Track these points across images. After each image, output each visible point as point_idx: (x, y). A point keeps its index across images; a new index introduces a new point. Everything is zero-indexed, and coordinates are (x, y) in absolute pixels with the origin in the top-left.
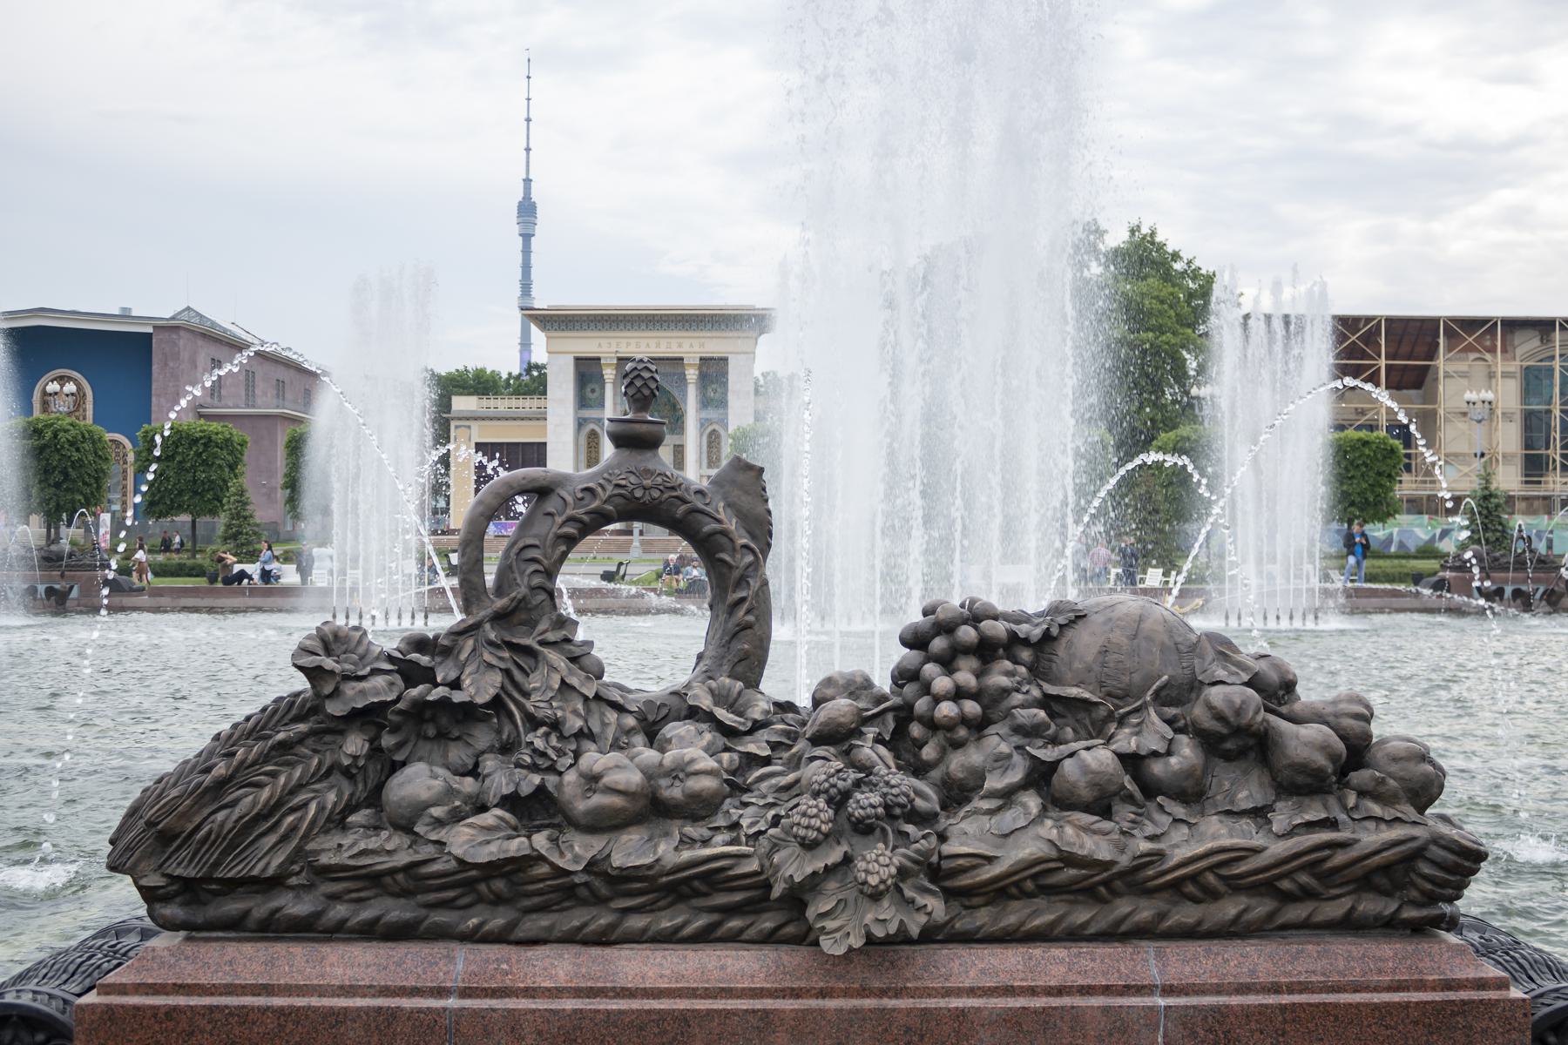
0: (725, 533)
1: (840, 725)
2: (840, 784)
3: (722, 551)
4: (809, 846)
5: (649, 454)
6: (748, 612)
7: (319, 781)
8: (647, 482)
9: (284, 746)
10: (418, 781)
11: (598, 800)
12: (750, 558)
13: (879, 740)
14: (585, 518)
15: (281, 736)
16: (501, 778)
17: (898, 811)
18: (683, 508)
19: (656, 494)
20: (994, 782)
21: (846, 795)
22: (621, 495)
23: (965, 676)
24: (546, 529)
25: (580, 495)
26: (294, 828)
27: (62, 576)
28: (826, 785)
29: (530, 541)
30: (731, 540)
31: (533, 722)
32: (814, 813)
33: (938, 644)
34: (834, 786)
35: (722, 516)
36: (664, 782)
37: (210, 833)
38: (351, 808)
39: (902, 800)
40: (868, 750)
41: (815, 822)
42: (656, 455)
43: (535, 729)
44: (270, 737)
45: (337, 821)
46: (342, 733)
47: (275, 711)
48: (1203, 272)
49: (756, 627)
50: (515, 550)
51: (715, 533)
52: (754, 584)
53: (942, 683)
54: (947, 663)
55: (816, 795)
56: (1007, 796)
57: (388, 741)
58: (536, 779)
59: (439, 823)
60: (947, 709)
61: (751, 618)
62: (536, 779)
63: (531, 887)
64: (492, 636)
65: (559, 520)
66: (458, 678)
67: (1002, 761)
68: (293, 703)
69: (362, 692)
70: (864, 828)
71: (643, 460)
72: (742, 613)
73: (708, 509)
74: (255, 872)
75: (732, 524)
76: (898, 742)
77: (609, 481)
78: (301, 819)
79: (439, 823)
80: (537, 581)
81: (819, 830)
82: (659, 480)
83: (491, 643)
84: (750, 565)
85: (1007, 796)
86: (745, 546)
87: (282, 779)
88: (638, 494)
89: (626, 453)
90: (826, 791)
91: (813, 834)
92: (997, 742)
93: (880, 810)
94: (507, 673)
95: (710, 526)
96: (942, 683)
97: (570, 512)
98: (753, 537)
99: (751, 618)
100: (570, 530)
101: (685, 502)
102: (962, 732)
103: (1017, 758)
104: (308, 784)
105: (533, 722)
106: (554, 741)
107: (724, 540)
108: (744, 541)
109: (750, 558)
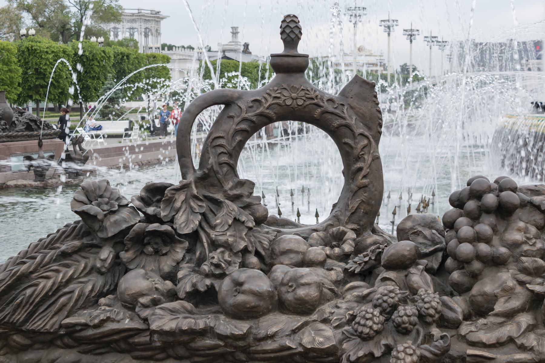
0: (347, 126)
1: (404, 256)
2: (390, 300)
3: (345, 137)
4: (365, 338)
5: (298, 75)
6: (365, 177)
7: (85, 276)
8: (294, 95)
9: (65, 255)
10: (136, 281)
11: (241, 298)
12: (366, 142)
13: (428, 270)
14: (254, 119)
15: (63, 247)
16: (188, 279)
17: (429, 319)
18: (319, 110)
19: (300, 102)
20: (499, 307)
21: (394, 307)
22: (277, 104)
23: (484, 228)
24: (231, 126)
25: (251, 104)
26: (64, 305)
27: (40, 145)
28: (380, 301)
29: (217, 135)
30: (352, 130)
31: (214, 245)
32: (371, 316)
33: (471, 205)
34: (385, 302)
35: (346, 115)
36: (283, 289)
37: (22, 301)
38: (102, 294)
39: (432, 311)
40: (417, 276)
41: (369, 323)
42: (303, 77)
43: (216, 249)
44: (59, 248)
45: (92, 301)
46: (101, 247)
47: (64, 232)
48: (231, 31)
49: (370, 186)
50: (210, 140)
51: (341, 126)
52: (368, 158)
53: (466, 230)
54: (475, 218)
55: (375, 306)
56: (510, 315)
57: (125, 256)
58: (208, 282)
59: (145, 306)
60: (466, 248)
61: (365, 181)
62: (208, 282)
63: (257, 356)
64: (195, 191)
65: (237, 120)
66: (200, 214)
67: (508, 292)
68: (76, 227)
69: (116, 223)
70: (403, 331)
71: (294, 80)
72: (360, 178)
73: (337, 111)
74: (48, 327)
75: (352, 121)
76: (438, 272)
77: (270, 95)
78: (70, 299)
79: (145, 306)
80: (224, 158)
81: (371, 328)
82: (303, 93)
83: (196, 197)
84: (365, 147)
85: (510, 315)
86: (362, 134)
87: (61, 275)
88: (289, 102)
89: (280, 75)
90: (380, 305)
91: (367, 330)
92: (507, 277)
93: (414, 319)
94: (203, 215)
95: (337, 122)
96: (466, 230)
97: (244, 115)
98: (369, 128)
99: (365, 181)
100: (243, 126)
101: (319, 106)
102: (477, 265)
103: (519, 289)
104: (78, 278)
105: (214, 245)
106: (227, 257)
107: (347, 131)
108: (361, 131)
109: (366, 142)
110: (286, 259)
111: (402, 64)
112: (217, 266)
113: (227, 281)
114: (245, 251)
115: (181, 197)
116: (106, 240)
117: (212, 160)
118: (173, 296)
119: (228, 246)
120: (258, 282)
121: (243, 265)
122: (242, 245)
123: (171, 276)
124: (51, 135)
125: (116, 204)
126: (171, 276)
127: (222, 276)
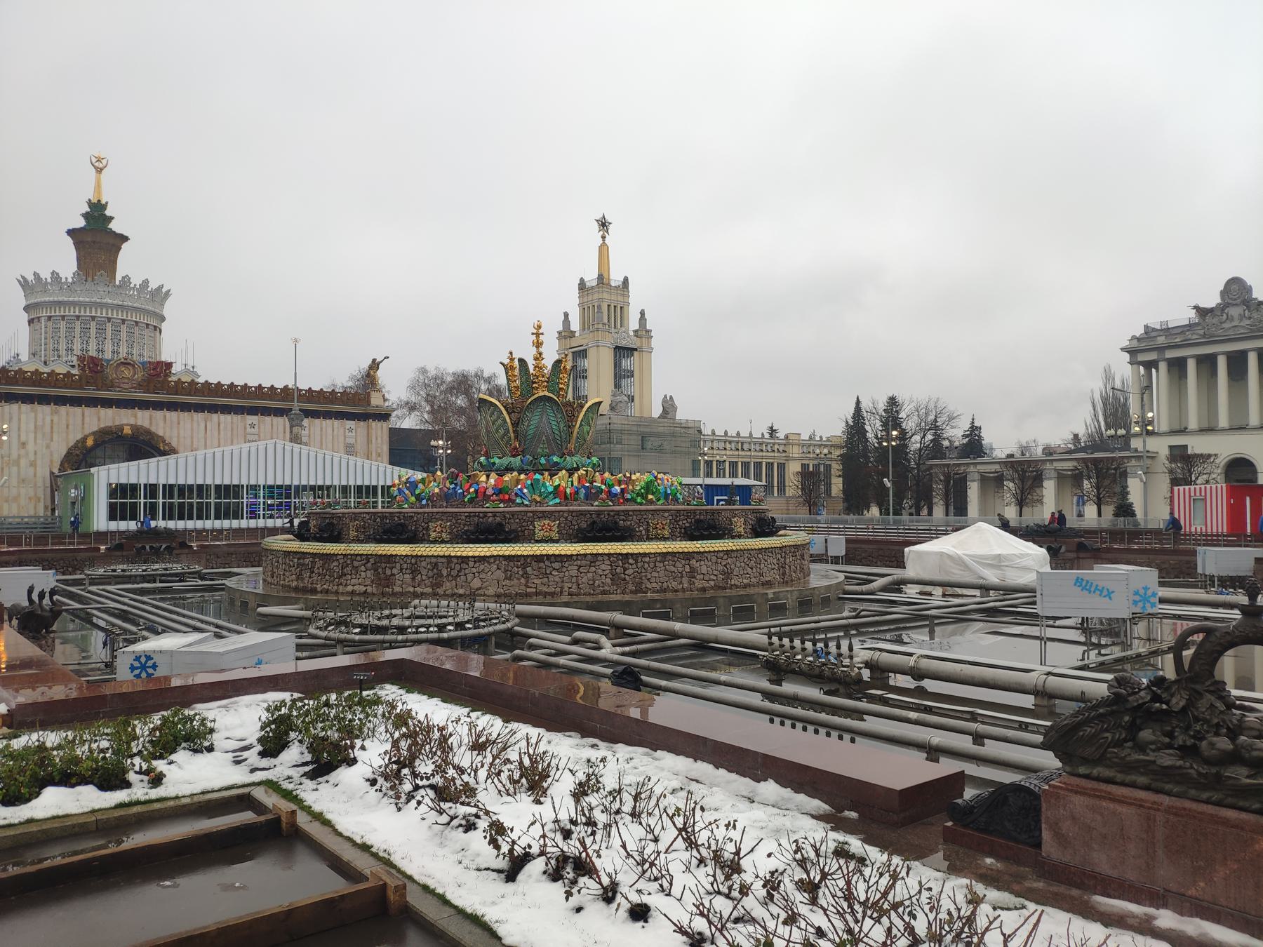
10: (1146, 735)
16: (1181, 739)
31: (1197, 719)
91: (1069, 465)
105: (1197, 719)
110: (1246, 732)
111: (599, 217)
112: (1199, 732)
113: (1204, 743)
114: (1218, 725)
115: (1174, 688)
116: (1127, 710)
117: (1197, 667)
118: (1169, 746)
119: (1206, 721)
120: (1224, 743)
121: (1217, 734)
122: (1216, 721)
123: (1170, 735)
124: (1110, 799)
125: (1134, 688)
126: (1170, 735)
127: (1203, 739)
